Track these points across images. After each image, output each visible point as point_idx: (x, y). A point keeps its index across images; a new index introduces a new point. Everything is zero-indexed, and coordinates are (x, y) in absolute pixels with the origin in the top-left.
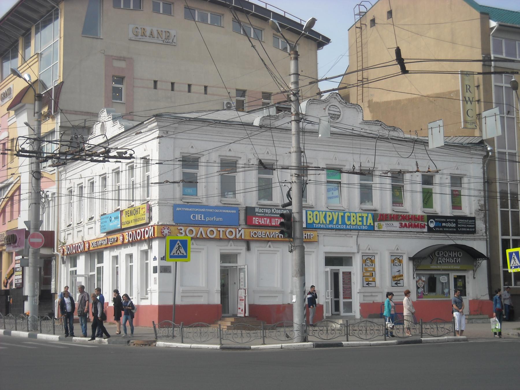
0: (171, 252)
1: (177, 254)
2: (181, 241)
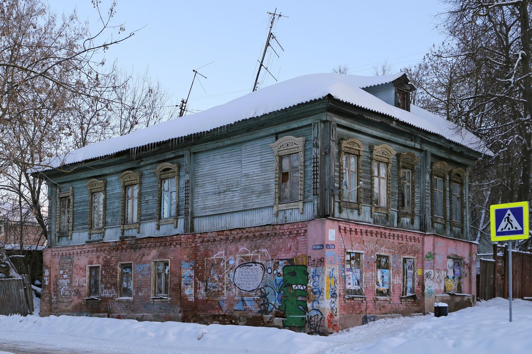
0: (498, 225)
1: (507, 230)
2: (512, 210)
